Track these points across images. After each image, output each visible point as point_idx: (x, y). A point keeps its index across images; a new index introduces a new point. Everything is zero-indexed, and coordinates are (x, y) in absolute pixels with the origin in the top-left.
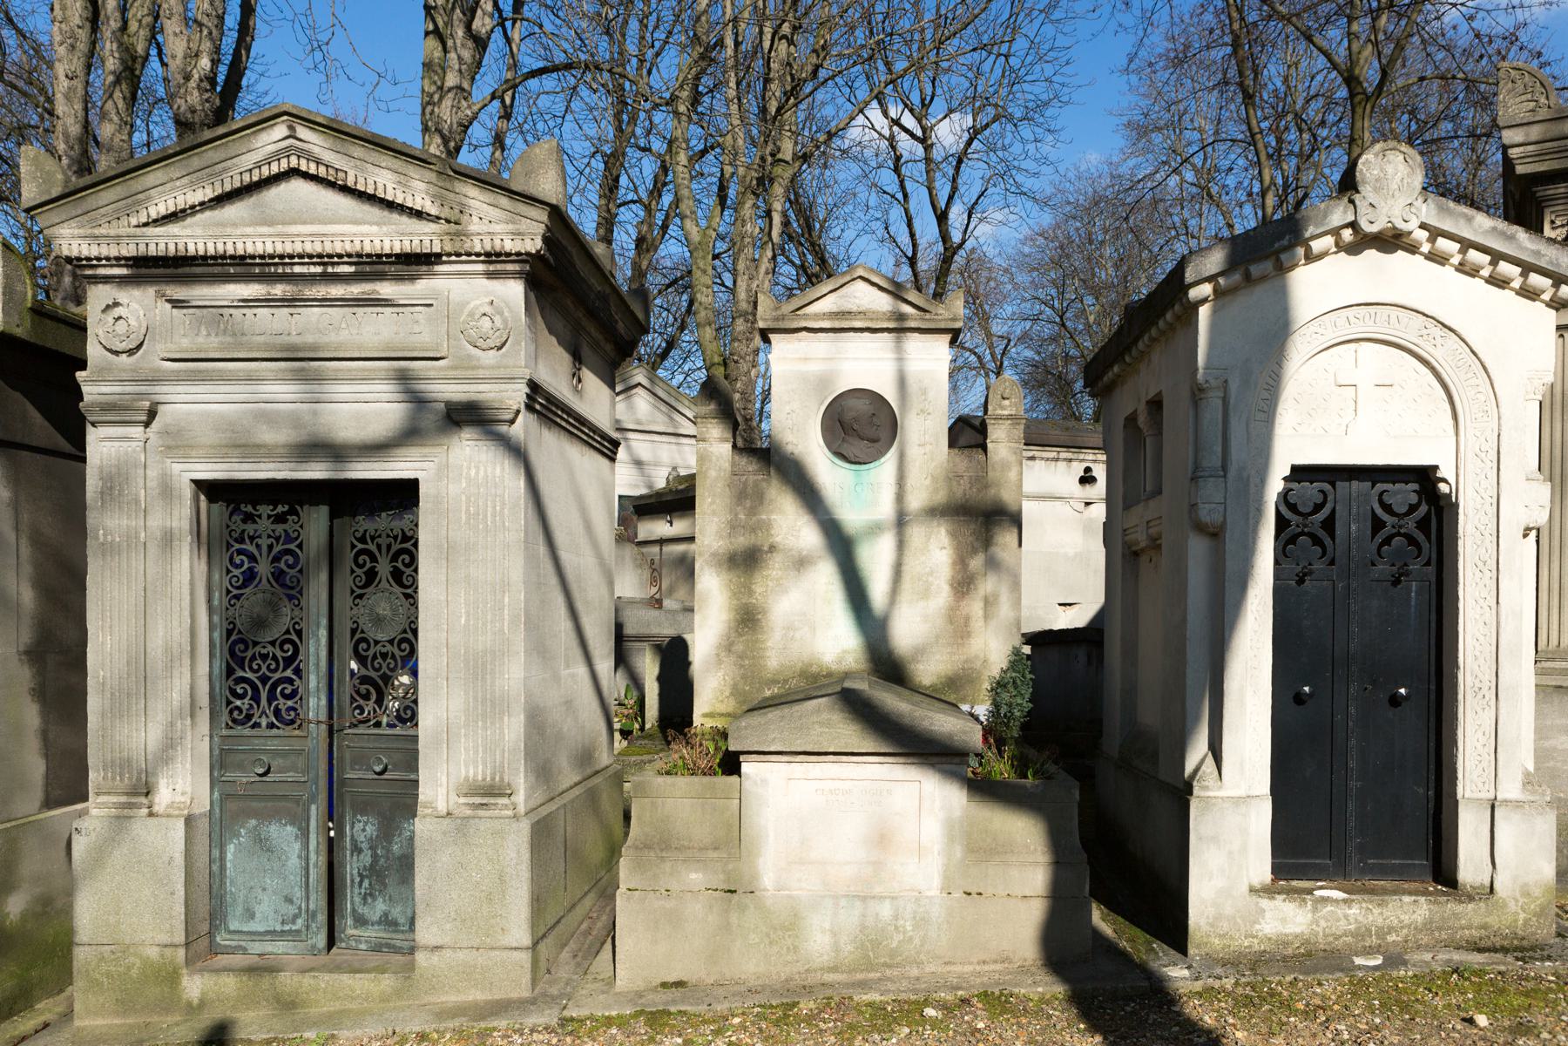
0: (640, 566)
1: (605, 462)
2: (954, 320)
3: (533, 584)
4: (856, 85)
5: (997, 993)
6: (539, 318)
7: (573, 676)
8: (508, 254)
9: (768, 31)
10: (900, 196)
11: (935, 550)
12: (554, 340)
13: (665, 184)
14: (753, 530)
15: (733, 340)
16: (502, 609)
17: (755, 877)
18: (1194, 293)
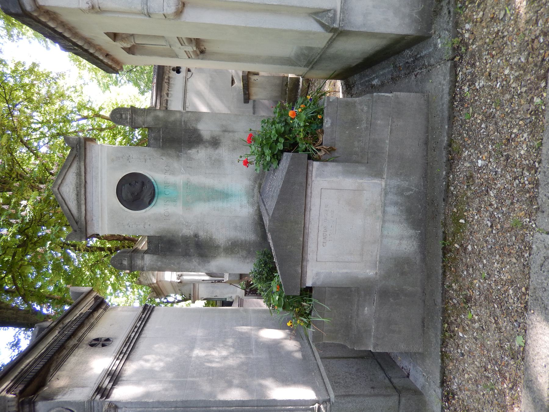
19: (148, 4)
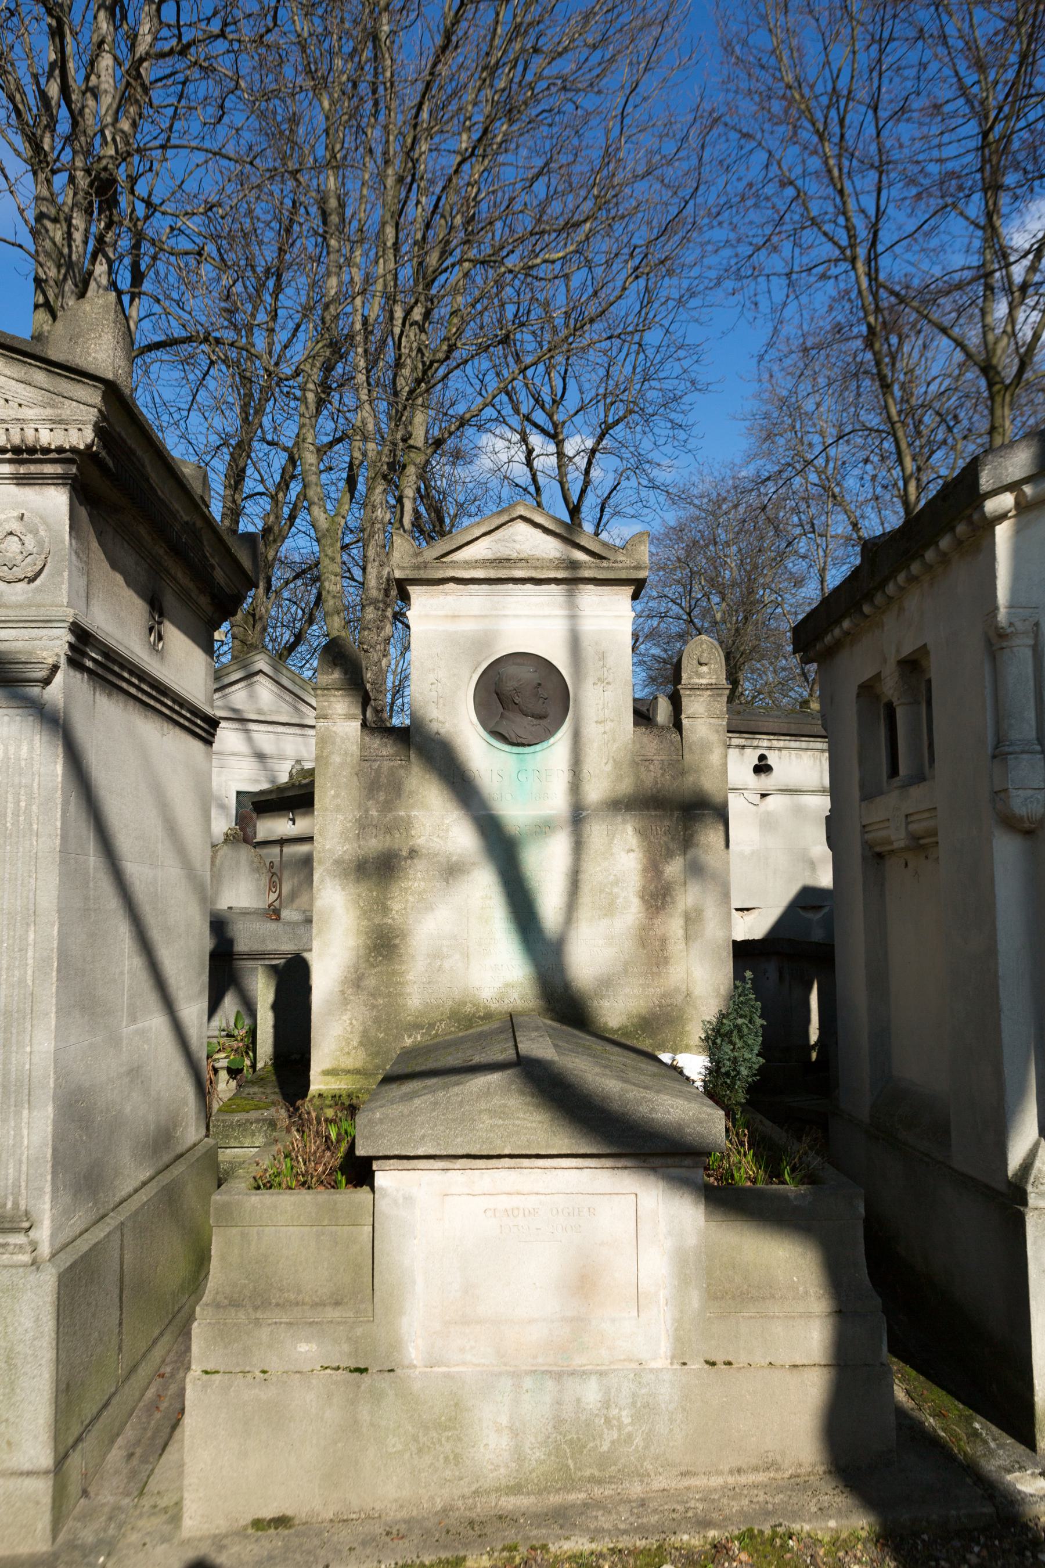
0: (257, 870)
1: (197, 745)
2: (638, 568)
3: (75, 912)
4: (487, 378)
5: (768, 1532)
6: (95, 545)
7: (142, 1033)
8: (46, 451)
9: (399, 313)
10: (532, 489)
11: (621, 854)
12: (119, 578)
13: (293, 477)
14: (389, 830)
15: (364, 629)
16: (23, 950)
17: (396, 1345)
18: (991, 506)
19: (1025, 756)
